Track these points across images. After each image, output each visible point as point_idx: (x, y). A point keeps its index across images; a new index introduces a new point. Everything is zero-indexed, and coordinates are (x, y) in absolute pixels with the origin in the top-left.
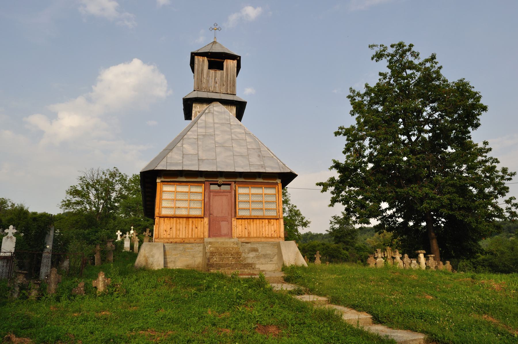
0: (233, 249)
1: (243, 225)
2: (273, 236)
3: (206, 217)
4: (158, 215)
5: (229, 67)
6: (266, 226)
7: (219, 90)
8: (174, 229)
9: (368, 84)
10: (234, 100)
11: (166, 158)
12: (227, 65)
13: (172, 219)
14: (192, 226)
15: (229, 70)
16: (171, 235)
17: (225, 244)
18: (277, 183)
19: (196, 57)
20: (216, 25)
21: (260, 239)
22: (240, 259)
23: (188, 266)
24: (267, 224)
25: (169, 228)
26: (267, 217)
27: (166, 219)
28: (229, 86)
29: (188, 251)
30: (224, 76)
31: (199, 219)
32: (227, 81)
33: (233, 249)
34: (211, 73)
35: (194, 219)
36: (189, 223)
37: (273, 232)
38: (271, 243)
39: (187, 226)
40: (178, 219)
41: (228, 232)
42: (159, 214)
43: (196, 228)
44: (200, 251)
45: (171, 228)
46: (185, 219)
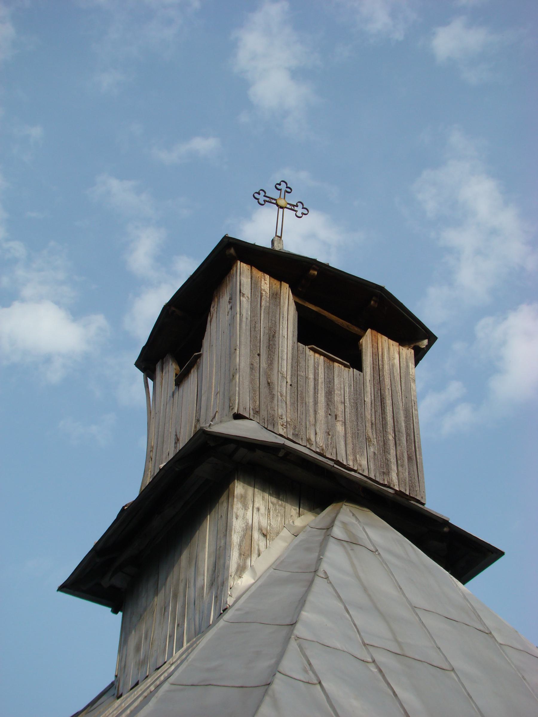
5: (386, 367)
7: (351, 458)
10: (446, 523)
12: (375, 355)
15: (388, 387)
28: (393, 452)
30: (368, 399)
32: (379, 426)
34: (311, 362)
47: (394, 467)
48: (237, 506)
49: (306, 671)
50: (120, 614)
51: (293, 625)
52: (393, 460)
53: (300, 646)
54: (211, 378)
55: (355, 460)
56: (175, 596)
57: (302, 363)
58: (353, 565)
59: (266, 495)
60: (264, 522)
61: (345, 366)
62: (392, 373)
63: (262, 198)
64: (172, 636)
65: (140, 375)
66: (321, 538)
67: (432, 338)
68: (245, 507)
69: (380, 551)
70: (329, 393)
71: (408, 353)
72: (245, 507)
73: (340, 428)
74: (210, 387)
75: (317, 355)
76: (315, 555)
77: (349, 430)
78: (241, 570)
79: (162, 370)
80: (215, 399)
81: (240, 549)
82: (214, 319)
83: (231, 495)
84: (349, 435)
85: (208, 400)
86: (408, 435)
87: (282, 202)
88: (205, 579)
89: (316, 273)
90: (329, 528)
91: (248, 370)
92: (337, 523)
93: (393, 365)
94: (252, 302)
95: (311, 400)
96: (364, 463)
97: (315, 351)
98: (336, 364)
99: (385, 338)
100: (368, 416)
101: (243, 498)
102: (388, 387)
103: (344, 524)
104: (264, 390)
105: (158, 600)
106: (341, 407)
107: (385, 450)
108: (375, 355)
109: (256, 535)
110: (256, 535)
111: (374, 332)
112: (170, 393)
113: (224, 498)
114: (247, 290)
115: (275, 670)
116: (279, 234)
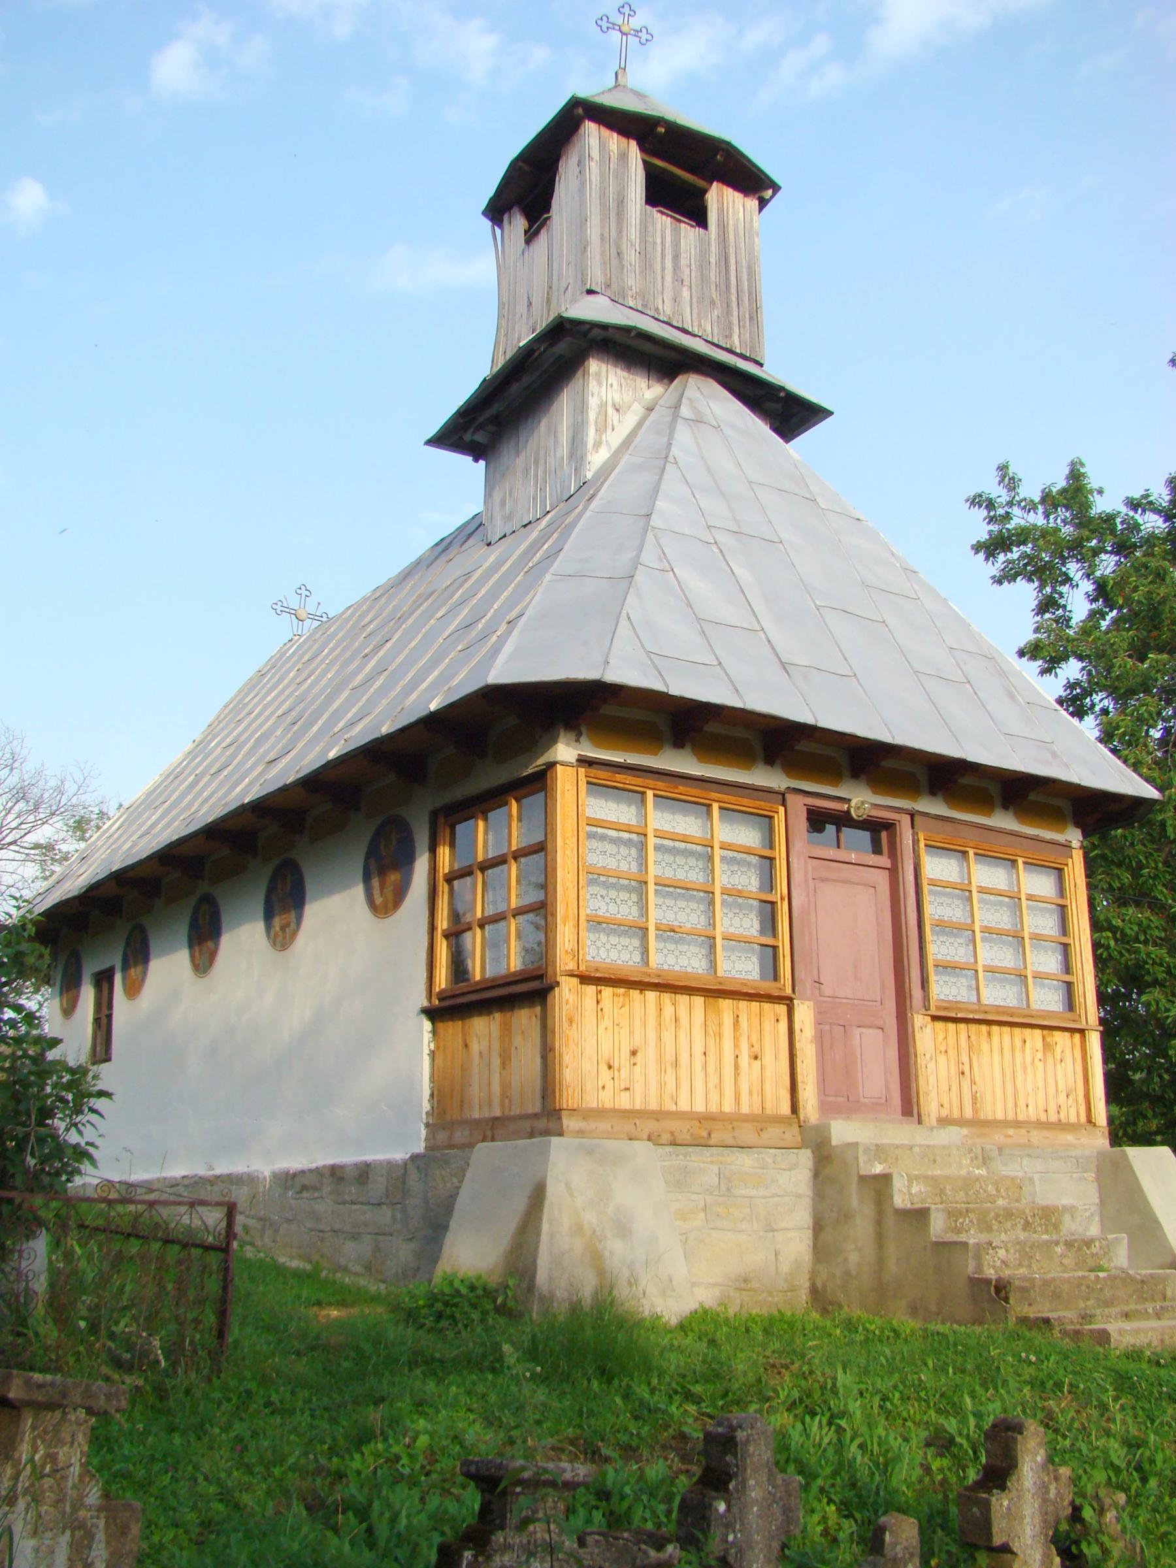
0: (998, 1191)
1: (950, 1051)
2: (1063, 1116)
3: (802, 999)
4: (571, 966)
5: (731, 223)
6: (1036, 1061)
7: (696, 324)
8: (649, 1056)
9: (1082, 465)
10: (782, 389)
11: (623, 622)
12: (721, 210)
13: (635, 994)
14: (736, 1045)
15: (732, 244)
16: (638, 1089)
17: (938, 1160)
18: (1067, 846)
19: (591, 131)
20: (626, 10)
21: (1023, 1131)
22: (1094, 1250)
23: (745, 1281)
24: (1040, 1055)
25: (626, 1052)
26: (1003, 1013)
27: (607, 992)
28: (735, 313)
29: (743, 1192)
30: (713, 260)
31: (767, 1006)
32: (723, 287)
33: (998, 1191)
34: (659, 226)
35: (743, 1004)
36: (720, 1025)
37: (1063, 1096)
38: (1073, 1153)
39: (711, 1042)
40: (667, 998)
41: (887, 1087)
42: (576, 954)
43: (756, 1058)
44: (799, 1196)
45: (634, 1053)
46: (699, 1001)
47: (736, 329)
48: (593, 385)
49: (661, 560)
50: (482, 463)
51: (649, 515)
52: (735, 322)
53: (655, 536)
54: (562, 246)
55: (700, 325)
56: (536, 462)
57: (650, 228)
58: (698, 444)
59: (619, 371)
60: (617, 398)
61: (692, 226)
62: (736, 229)
63: (604, 25)
64: (535, 498)
65: (487, 224)
66: (669, 419)
67: (776, 188)
68: (600, 384)
69: (722, 427)
70: (676, 257)
71: (752, 203)
72: (600, 384)
73: (686, 293)
74: (561, 255)
75: (664, 217)
76: (665, 439)
77: (694, 294)
78: (598, 445)
79: (510, 223)
80: (567, 269)
81: (596, 425)
82: (562, 180)
83: (586, 374)
84: (695, 300)
85: (561, 267)
86: (750, 294)
87: (625, 29)
88: (564, 450)
89: (663, 130)
90: (677, 407)
91: (599, 241)
92: (684, 400)
93: (738, 220)
94: (601, 166)
95: (658, 267)
96: (709, 328)
97: (662, 213)
98: (683, 225)
99: (730, 190)
100: (713, 278)
101: (598, 374)
102: (732, 244)
103: (689, 399)
104: (615, 261)
105: (520, 462)
106: (687, 271)
107: (728, 312)
108: (721, 210)
109: (610, 410)
110: (610, 410)
111: (720, 185)
112: (520, 251)
113: (579, 374)
114: (595, 154)
115: (636, 563)
116: (623, 65)
